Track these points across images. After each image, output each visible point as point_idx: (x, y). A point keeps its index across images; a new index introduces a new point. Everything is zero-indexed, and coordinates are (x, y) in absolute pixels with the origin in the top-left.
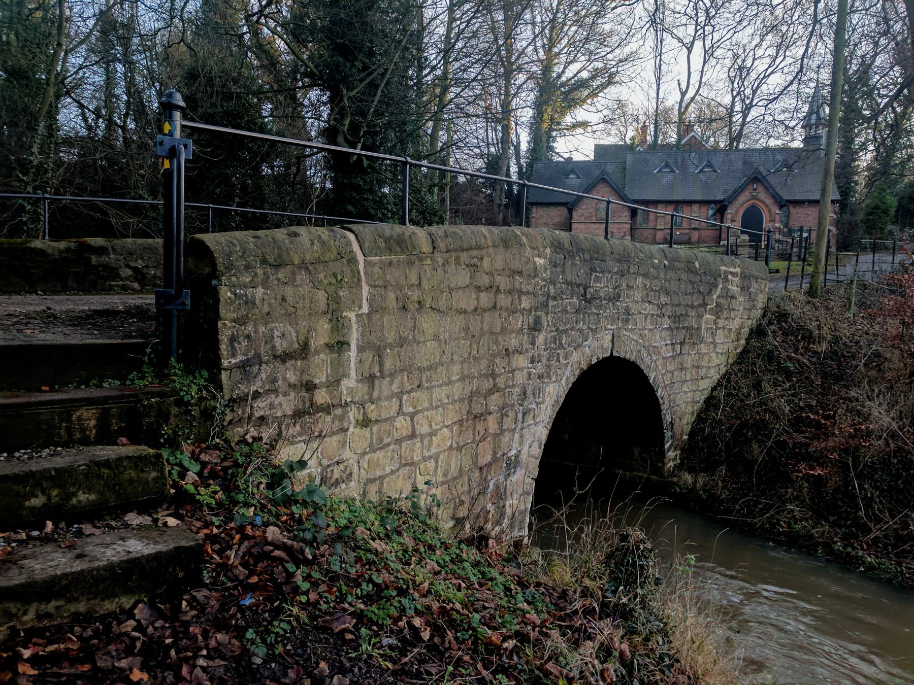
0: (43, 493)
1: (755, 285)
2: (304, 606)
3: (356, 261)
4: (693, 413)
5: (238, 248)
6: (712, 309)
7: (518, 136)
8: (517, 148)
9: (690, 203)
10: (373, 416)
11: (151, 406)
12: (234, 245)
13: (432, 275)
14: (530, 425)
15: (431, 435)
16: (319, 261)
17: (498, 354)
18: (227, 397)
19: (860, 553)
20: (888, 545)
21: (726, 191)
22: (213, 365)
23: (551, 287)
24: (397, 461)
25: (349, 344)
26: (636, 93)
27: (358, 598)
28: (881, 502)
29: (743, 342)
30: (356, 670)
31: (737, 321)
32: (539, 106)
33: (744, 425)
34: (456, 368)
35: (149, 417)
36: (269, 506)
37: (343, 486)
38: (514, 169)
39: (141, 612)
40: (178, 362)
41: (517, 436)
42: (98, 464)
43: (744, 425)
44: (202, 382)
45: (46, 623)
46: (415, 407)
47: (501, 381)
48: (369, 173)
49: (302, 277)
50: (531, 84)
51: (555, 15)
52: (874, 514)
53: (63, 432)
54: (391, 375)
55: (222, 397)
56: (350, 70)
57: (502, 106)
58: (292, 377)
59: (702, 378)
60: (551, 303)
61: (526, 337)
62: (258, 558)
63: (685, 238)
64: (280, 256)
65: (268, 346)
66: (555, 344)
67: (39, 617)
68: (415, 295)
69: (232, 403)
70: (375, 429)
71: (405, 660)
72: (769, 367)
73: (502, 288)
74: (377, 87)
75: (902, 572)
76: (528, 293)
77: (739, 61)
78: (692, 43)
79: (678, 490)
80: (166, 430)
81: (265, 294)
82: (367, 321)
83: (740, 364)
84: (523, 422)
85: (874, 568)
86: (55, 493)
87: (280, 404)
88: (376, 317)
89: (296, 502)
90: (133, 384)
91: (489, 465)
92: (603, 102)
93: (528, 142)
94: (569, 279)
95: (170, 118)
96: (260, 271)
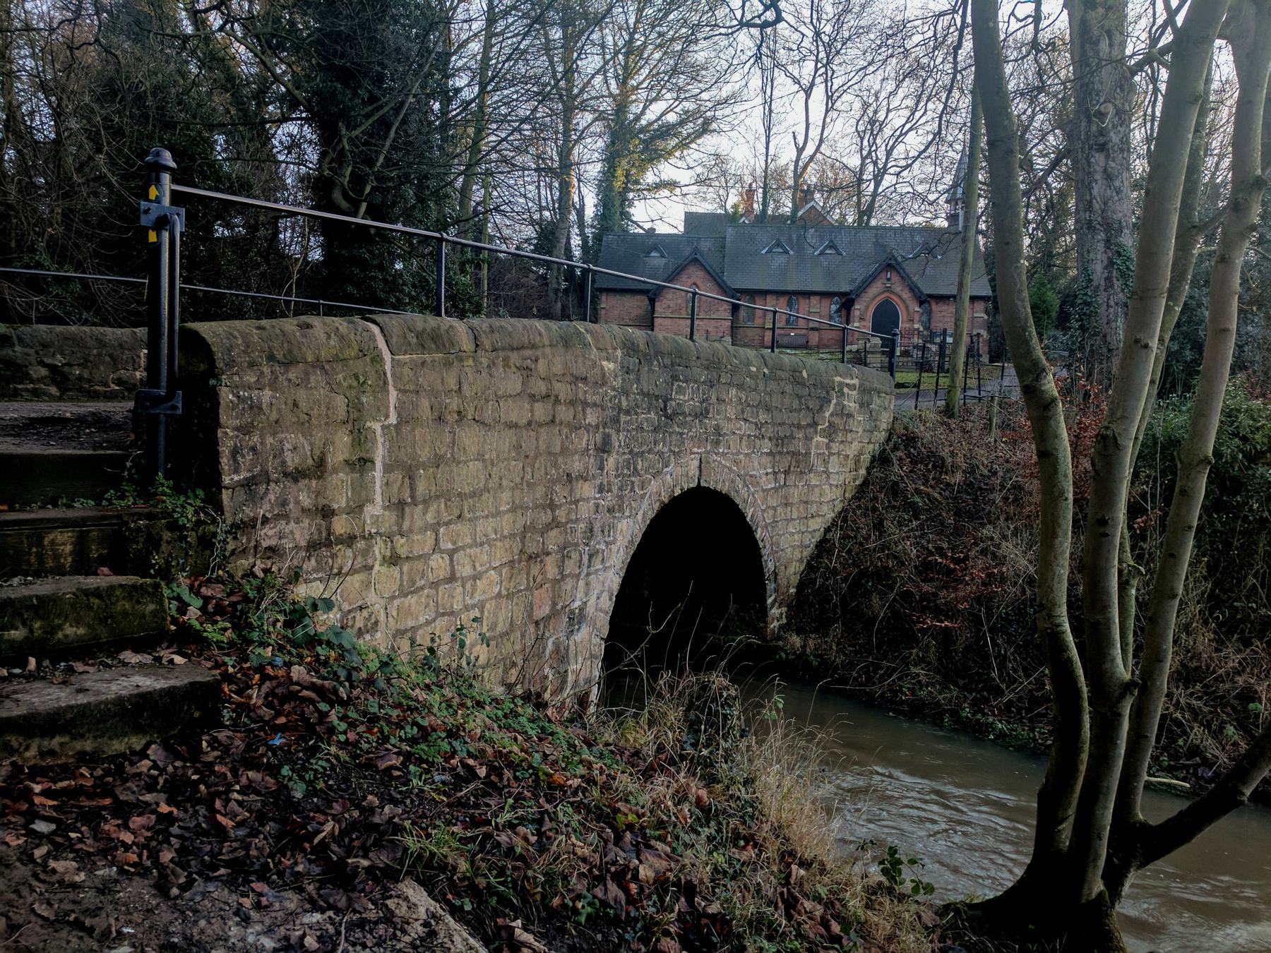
0: (24, 624)
1: (876, 402)
2: (342, 745)
3: (382, 359)
4: (801, 560)
5: (240, 342)
6: (824, 430)
7: (582, 199)
8: (581, 213)
9: (808, 294)
10: (403, 552)
11: (138, 530)
12: (235, 337)
13: (475, 379)
14: (598, 570)
15: (475, 578)
16: (337, 359)
17: (558, 480)
18: (229, 522)
19: (991, 719)
20: (1022, 709)
21: (854, 281)
22: (212, 482)
23: (623, 398)
24: (433, 609)
25: (373, 462)
26: (740, 146)
27: (401, 740)
28: (1015, 659)
29: (863, 472)
30: (408, 801)
31: (856, 446)
32: (611, 159)
33: (863, 574)
34: (506, 496)
35: (137, 543)
36: (288, 647)
37: (368, 637)
38: (576, 241)
39: (155, 752)
40: (166, 478)
41: (581, 583)
42: (87, 593)
43: (863, 574)
44: (198, 503)
45: (49, 761)
46: (454, 543)
47: (561, 514)
48: (377, 243)
49: (317, 378)
50: (598, 127)
51: (632, 35)
52: (1008, 674)
53: (33, 559)
54: (425, 502)
55: (224, 522)
56: (351, 100)
57: (560, 154)
58: (306, 500)
59: (813, 517)
60: (623, 418)
61: (592, 460)
62: (284, 699)
63: (802, 341)
64: (290, 352)
65: (277, 461)
66: (629, 469)
67: (42, 754)
68: (454, 403)
69: (238, 528)
70: (406, 568)
71: (459, 794)
72: (894, 503)
73: (562, 397)
74: (388, 126)
75: (1034, 739)
76: (595, 405)
77: (870, 112)
78: (812, 85)
79: (783, 655)
80: (156, 559)
81: (273, 397)
82: (395, 434)
83: (860, 499)
84: (589, 567)
85: (1005, 735)
86: (37, 625)
87: (292, 532)
88: (406, 429)
89: (320, 643)
90: (111, 504)
91: (547, 619)
92: (696, 155)
93: (596, 206)
94: (645, 390)
95: (158, 181)
96: (266, 370)
